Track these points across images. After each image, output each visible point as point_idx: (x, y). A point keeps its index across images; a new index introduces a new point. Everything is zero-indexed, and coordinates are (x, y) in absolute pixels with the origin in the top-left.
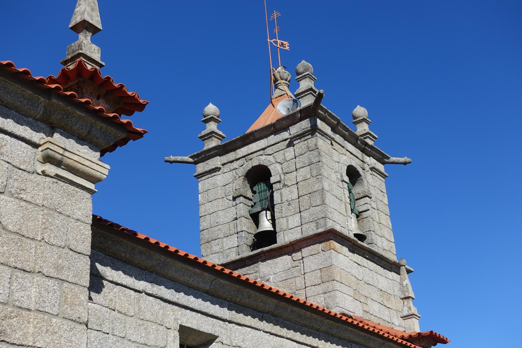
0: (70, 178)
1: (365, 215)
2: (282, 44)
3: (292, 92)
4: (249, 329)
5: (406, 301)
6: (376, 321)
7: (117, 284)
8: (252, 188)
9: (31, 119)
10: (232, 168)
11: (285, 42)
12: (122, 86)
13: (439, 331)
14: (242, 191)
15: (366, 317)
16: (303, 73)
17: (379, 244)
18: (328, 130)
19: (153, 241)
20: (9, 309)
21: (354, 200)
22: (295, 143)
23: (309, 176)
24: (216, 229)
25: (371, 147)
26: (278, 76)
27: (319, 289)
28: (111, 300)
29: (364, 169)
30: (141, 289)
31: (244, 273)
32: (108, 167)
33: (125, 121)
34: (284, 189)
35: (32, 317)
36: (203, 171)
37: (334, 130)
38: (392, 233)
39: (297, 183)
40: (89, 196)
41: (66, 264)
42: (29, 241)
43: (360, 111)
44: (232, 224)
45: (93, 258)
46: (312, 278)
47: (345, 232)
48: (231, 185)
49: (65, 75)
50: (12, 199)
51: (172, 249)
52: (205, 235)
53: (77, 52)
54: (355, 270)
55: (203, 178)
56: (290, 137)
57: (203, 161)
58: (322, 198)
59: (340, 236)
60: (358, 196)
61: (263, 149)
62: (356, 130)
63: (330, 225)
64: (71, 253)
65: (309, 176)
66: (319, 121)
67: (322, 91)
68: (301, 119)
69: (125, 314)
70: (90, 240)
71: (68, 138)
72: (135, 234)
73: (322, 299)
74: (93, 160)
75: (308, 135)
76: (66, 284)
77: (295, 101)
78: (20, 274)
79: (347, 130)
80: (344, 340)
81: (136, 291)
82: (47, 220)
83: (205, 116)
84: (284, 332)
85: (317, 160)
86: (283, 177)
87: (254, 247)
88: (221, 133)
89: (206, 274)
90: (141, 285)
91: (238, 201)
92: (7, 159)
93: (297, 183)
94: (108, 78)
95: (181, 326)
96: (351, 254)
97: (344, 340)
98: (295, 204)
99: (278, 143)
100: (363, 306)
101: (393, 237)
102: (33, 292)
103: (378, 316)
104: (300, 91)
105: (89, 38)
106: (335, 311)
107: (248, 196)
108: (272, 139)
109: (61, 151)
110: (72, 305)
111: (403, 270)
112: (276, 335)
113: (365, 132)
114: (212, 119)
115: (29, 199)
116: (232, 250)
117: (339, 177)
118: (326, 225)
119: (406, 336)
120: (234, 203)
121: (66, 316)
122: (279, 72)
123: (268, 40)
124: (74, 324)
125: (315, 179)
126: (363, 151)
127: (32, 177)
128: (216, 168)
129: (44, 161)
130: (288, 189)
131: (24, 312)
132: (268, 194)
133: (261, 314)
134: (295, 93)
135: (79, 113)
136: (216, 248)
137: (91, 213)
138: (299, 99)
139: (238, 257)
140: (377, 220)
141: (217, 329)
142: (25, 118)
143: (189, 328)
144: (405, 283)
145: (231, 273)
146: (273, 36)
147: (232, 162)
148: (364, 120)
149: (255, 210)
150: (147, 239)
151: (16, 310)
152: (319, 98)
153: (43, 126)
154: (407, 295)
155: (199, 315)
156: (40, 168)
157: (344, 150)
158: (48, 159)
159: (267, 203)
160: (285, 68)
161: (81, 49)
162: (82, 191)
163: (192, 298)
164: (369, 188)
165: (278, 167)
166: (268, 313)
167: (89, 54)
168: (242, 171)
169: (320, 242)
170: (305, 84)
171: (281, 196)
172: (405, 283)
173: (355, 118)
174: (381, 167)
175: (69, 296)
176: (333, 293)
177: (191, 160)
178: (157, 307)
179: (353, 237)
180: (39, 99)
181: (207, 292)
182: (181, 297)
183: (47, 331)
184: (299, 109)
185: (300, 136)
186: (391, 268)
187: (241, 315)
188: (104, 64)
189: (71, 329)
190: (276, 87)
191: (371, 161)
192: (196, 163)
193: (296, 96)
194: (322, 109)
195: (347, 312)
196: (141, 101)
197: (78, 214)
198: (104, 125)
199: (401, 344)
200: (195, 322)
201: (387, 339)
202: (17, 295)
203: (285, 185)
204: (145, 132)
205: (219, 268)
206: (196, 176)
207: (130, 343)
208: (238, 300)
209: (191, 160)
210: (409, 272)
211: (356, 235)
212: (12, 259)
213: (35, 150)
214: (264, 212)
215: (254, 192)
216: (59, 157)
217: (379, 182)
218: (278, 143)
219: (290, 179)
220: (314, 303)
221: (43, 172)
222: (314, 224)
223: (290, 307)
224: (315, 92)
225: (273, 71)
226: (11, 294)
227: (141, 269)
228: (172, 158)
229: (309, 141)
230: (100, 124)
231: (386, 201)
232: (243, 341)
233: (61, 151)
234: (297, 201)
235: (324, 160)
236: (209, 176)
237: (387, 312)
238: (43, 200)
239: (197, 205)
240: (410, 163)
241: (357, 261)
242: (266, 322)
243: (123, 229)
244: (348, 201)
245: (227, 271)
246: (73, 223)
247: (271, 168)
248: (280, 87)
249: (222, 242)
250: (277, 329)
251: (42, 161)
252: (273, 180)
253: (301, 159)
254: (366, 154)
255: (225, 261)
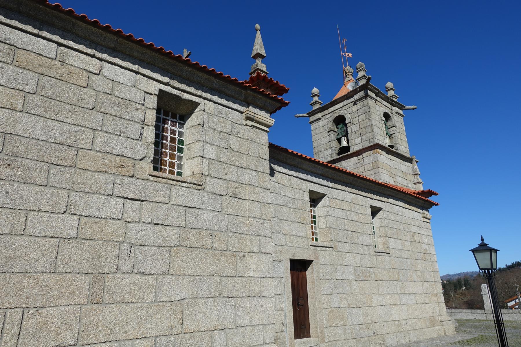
0: (258, 126)
1: (393, 136)
2: (348, 55)
3: (355, 78)
4: (341, 191)
5: (416, 176)
6: (400, 186)
7: (281, 172)
8: (337, 127)
9: (239, 101)
10: (327, 118)
11: (349, 54)
12: (277, 82)
13: (432, 189)
14: (332, 128)
15: (395, 184)
16: (360, 68)
17: (401, 149)
18: (373, 95)
19: (295, 153)
20: (238, 184)
21: (387, 129)
22: (357, 103)
23: (365, 119)
24: (320, 147)
25: (396, 102)
26: (347, 71)
27: (372, 172)
28: (279, 180)
29: (392, 113)
30: (291, 174)
31: (337, 165)
32: (274, 120)
33: (280, 98)
34: (353, 126)
35: (247, 187)
36: (313, 120)
37: (377, 95)
38: (407, 144)
39: (359, 123)
40: (266, 134)
41: (259, 164)
42: (243, 155)
43: (389, 85)
44: (328, 144)
45: (270, 161)
46: (370, 167)
47: (384, 144)
48: (326, 126)
49: (252, 80)
50: (234, 137)
51: (304, 156)
52: (316, 150)
53: (256, 68)
54: (389, 162)
55: (313, 123)
56: (355, 100)
57: (312, 115)
58: (372, 129)
59: (381, 146)
60: (390, 127)
61: (341, 107)
62: (387, 95)
63: (376, 141)
64: (261, 159)
65: (365, 119)
66: (368, 91)
67: (370, 76)
68: (360, 91)
69: (285, 186)
70: (268, 153)
71: (255, 108)
72: (287, 150)
73: (373, 176)
74: (267, 117)
75: (363, 99)
76: (260, 173)
77: (356, 83)
78: (241, 169)
79: (383, 95)
80: (386, 195)
81: (289, 175)
82: (250, 145)
83: (312, 94)
84: (357, 192)
85: (369, 111)
86: (352, 120)
87: (339, 154)
88: (320, 101)
89: (320, 167)
90: (291, 172)
91: (330, 133)
92: (231, 120)
93: (359, 123)
94: (271, 79)
95: (310, 190)
96: (387, 155)
97: (386, 195)
98: (358, 133)
99: (349, 104)
100: (394, 179)
101: (408, 146)
102: (247, 177)
103: (401, 184)
104: (359, 77)
105: (261, 61)
106: (380, 181)
107: (335, 130)
108: (346, 102)
109: (253, 114)
110: (263, 182)
111: (414, 161)
112: (353, 193)
113: (392, 95)
114: (316, 95)
115: (241, 136)
116: (329, 156)
117: (380, 118)
118: (374, 142)
119: (416, 192)
120: (329, 134)
121: (261, 187)
122: (347, 69)
123: (341, 54)
124: (265, 190)
125: (368, 120)
126: (392, 104)
127: (242, 127)
128: (319, 118)
129: (246, 119)
130: (354, 126)
131: (244, 185)
132: (345, 129)
133: (346, 184)
134: (356, 79)
135: (259, 96)
136: (321, 156)
137: (268, 141)
138: (358, 81)
139: (332, 159)
140: (400, 137)
141: (326, 191)
142: (236, 100)
143: (313, 191)
144: (415, 167)
145: (331, 166)
146: (343, 52)
147: (326, 115)
148: (392, 89)
149: (339, 137)
150: (293, 152)
151: (240, 185)
152: (369, 80)
153: (244, 103)
154: (416, 173)
155: (317, 185)
156: (245, 123)
157: (382, 105)
158: (248, 118)
159: (344, 133)
160: (350, 67)
161: (258, 67)
162: (263, 132)
163: (314, 178)
164: (395, 122)
165: (349, 115)
166: (349, 183)
167: (261, 69)
168: (332, 119)
169: (372, 150)
170: (361, 74)
171: (351, 129)
172: (415, 167)
173: (387, 88)
174: (401, 112)
175: (262, 178)
176: (378, 174)
177: (307, 115)
178: (298, 182)
179: (388, 147)
180: (242, 91)
181: (320, 175)
182: (309, 177)
183: (254, 193)
184: (358, 86)
185: (360, 100)
186: (407, 160)
187: (337, 185)
188: (268, 72)
189: (264, 192)
190: (346, 77)
191: (396, 109)
192: (309, 117)
193: (357, 80)
194: (370, 85)
195: (386, 182)
196: (286, 88)
197: (263, 142)
198: (271, 101)
199: (414, 196)
200: (316, 188)
201: (407, 194)
202: (240, 178)
203: (353, 124)
204: (289, 103)
205: (326, 164)
206: (309, 123)
207: (288, 198)
208: (335, 178)
209: (307, 115)
210: (417, 162)
211: (389, 146)
212: (237, 163)
213: (242, 115)
214: (343, 137)
215: (338, 128)
216: (252, 117)
217: (400, 119)
218: (349, 104)
219: (355, 121)
220: (364, 176)
221: (246, 124)
222: (368, 142)
223: (359, 180)
224: (366, 77)
225: (345, 69)
226: (238, 177)
227: (290, 165)
228: (298, 115)
229: (364, 101)
230: (269, 101)
231: (404, 128)
232: (338, 196)
233: (253, 114)
234: (359, 131)
235: (372, 110)
236: (316, 122)
237: (405, 181)
238: (247, 137)
239: (311, 136)
240: (416, 108)
241: (390, 158)
242: (349, 187)
243: (282, 148)
244: (385, 129)
245: (329, 165)
246: (261, 146)
247: (346, 116)
248: (348, 76)
249: (324, 153)
250: (353, 191)
251: (245, 119)
252: (347, 122)
253: (360, 111)
254: (393, 106)
255: (327, 160)
